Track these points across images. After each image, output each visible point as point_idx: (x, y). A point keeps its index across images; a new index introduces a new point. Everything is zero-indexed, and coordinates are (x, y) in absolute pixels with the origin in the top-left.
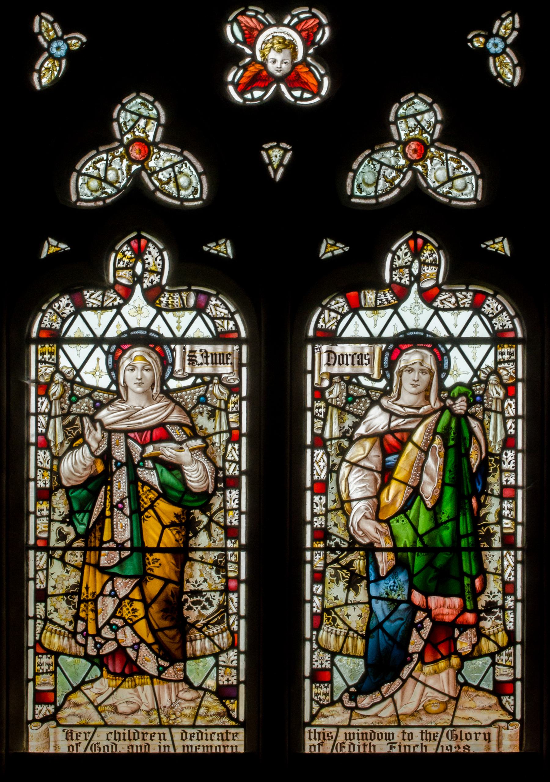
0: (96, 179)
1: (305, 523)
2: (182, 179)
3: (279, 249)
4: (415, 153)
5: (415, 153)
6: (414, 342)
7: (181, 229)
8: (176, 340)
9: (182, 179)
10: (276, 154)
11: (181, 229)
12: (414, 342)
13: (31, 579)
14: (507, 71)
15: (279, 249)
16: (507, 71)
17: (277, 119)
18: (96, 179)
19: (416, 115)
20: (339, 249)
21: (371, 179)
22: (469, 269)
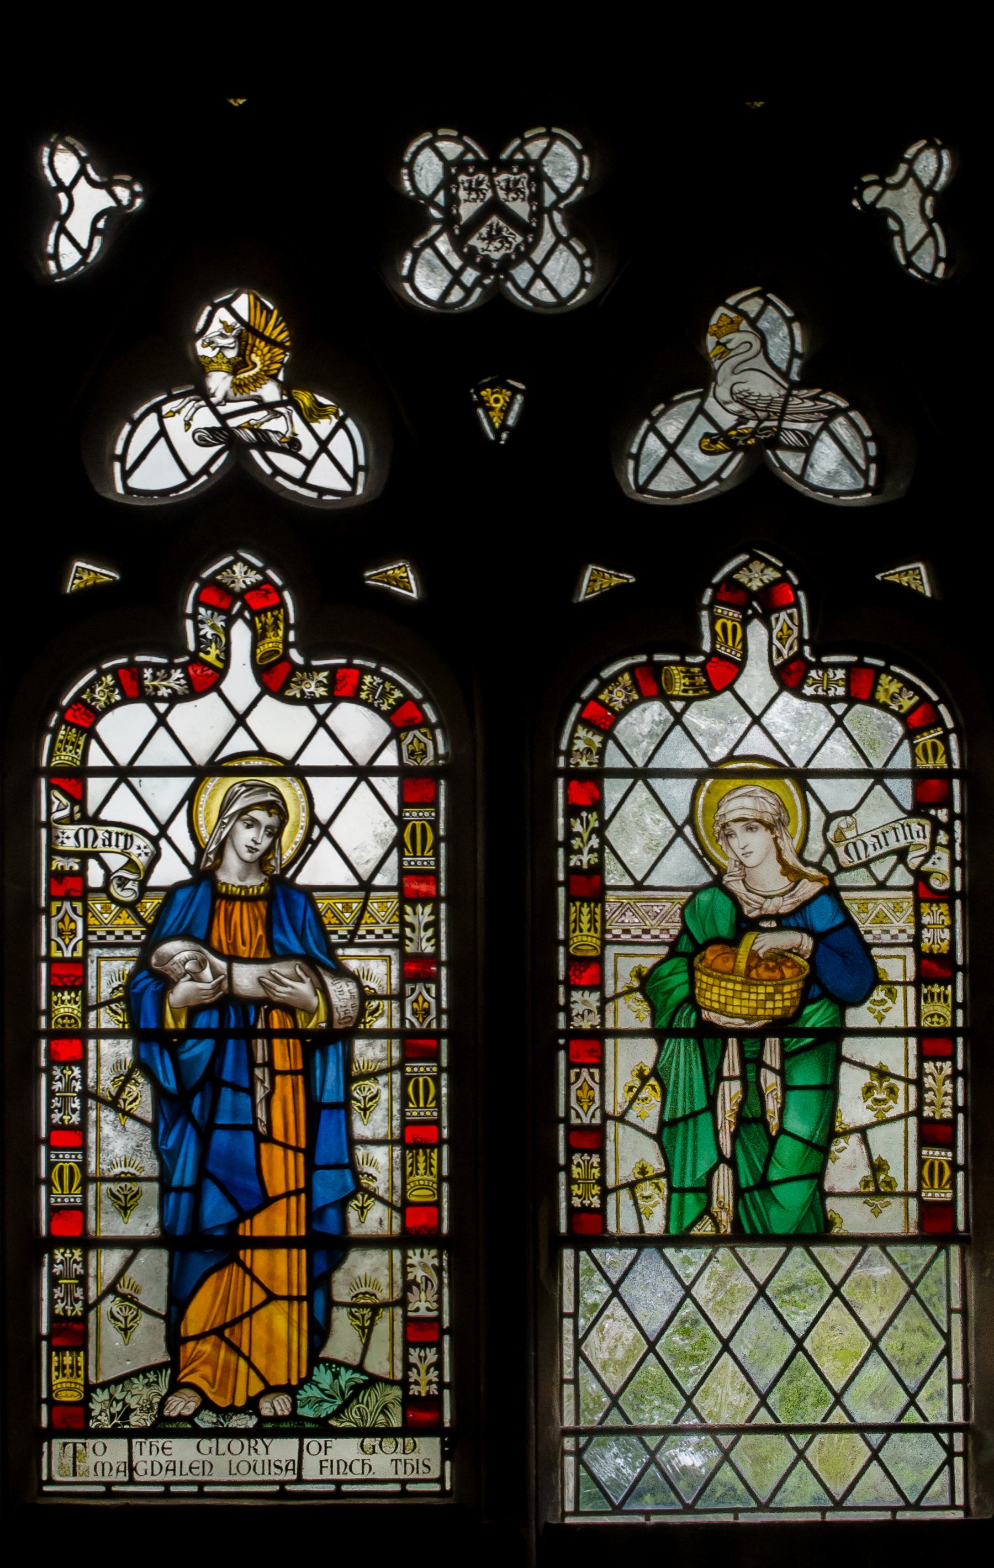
0: (163, 453)
1: (448, 1070)
2: (327, 458)
3: (501, 599)
4: (752, 400)
5: (752, 400)
6: (747, 772)
7: (318, 553)
8: (660, 1242)
9: (327, 458)
10: (495, 398)
11: (318, 553)
12: (747, 772)
13: (568, 1315)
14: (920, 244)
15: (501, 599)
16: (920, 244)
17: (497, 330)
18: (163, 453)
19: (755, 349)
20: (612, 579)
21: (675, 456)
22: (852, 632)
